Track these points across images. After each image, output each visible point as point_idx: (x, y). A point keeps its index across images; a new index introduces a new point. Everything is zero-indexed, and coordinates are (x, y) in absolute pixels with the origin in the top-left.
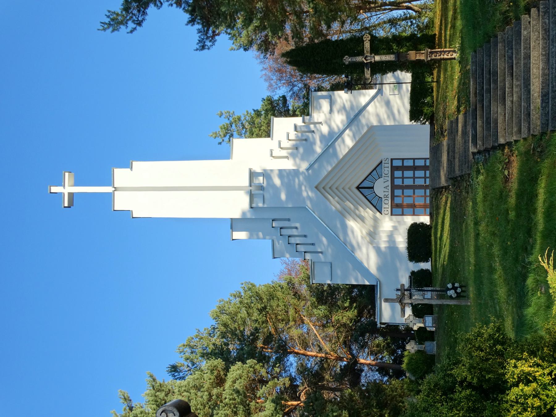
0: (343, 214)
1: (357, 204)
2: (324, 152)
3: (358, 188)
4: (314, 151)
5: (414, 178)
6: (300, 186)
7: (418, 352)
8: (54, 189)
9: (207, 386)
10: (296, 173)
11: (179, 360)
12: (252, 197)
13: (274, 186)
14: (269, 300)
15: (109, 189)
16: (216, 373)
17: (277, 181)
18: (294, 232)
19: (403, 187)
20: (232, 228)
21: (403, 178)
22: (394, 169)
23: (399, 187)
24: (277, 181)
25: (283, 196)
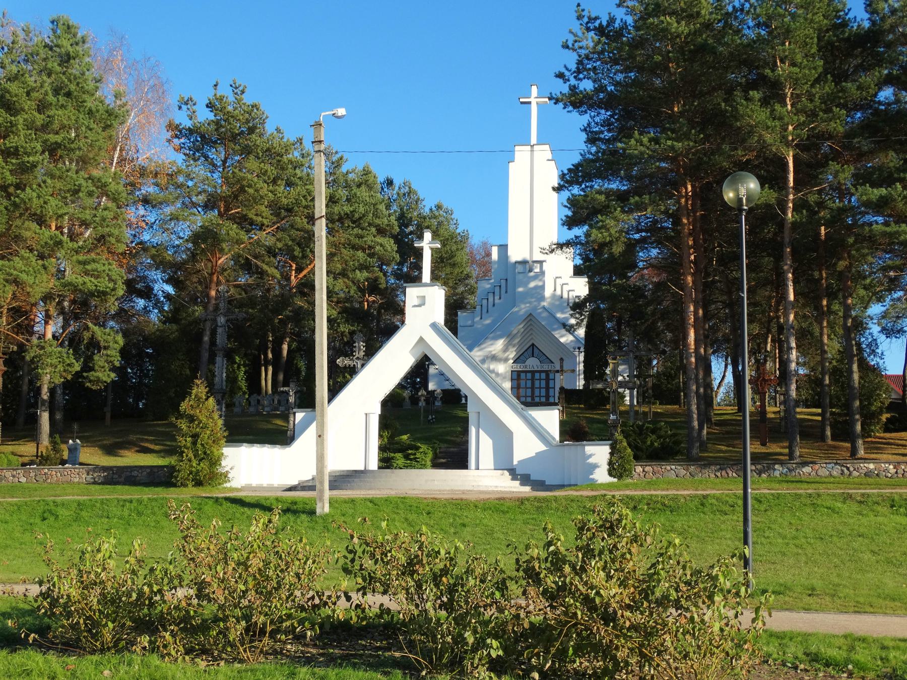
0: (510, 337)
1: (520, 344)
2: (557, 320)
3: (533, 345)
4: (557, 312)
5: (540, 388)
6: (530, 303)
7: (405, 398)
8: (534, 89)
9: (377, 221)
10: (543, 298)
11: (397, 182)
12: (524, 262)
13: (529, 283)
14: (450, 264)
15: (534, 140)
16: (388, 228)
17: (532, 284)
18: (497, 297)
19: (533, 380)
20: (501, 245)
21: (540, 379)
22: (547, 373)
23: (533, 376)
24: (532, 284)
25: (521, 289)
